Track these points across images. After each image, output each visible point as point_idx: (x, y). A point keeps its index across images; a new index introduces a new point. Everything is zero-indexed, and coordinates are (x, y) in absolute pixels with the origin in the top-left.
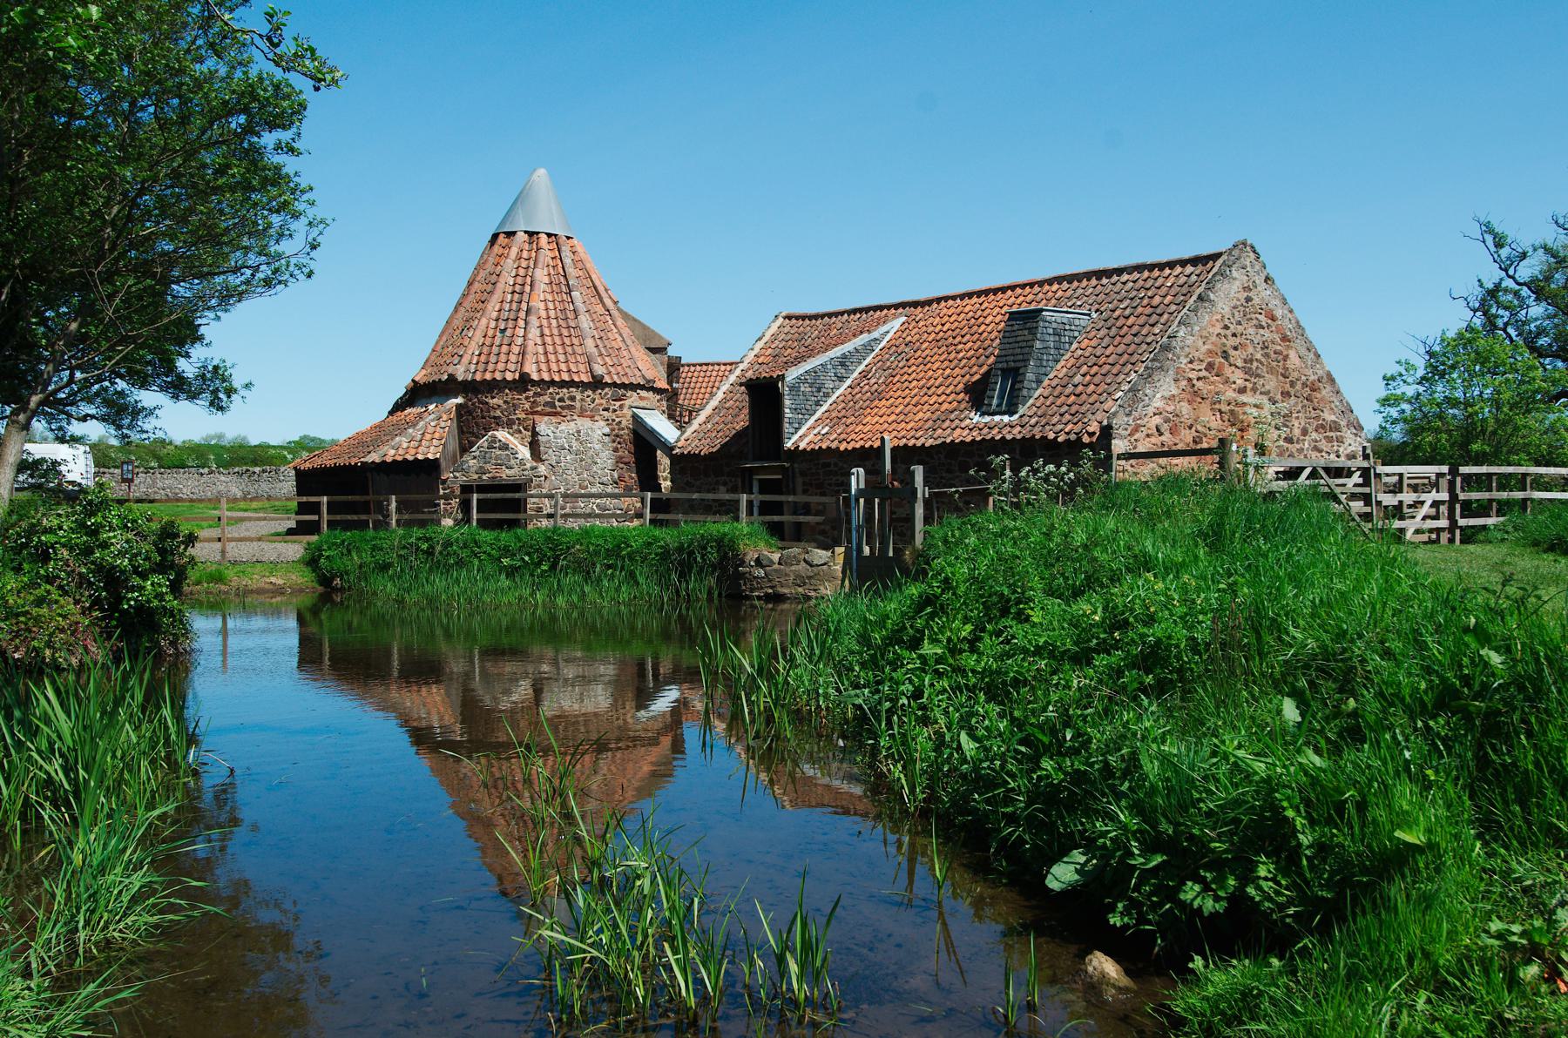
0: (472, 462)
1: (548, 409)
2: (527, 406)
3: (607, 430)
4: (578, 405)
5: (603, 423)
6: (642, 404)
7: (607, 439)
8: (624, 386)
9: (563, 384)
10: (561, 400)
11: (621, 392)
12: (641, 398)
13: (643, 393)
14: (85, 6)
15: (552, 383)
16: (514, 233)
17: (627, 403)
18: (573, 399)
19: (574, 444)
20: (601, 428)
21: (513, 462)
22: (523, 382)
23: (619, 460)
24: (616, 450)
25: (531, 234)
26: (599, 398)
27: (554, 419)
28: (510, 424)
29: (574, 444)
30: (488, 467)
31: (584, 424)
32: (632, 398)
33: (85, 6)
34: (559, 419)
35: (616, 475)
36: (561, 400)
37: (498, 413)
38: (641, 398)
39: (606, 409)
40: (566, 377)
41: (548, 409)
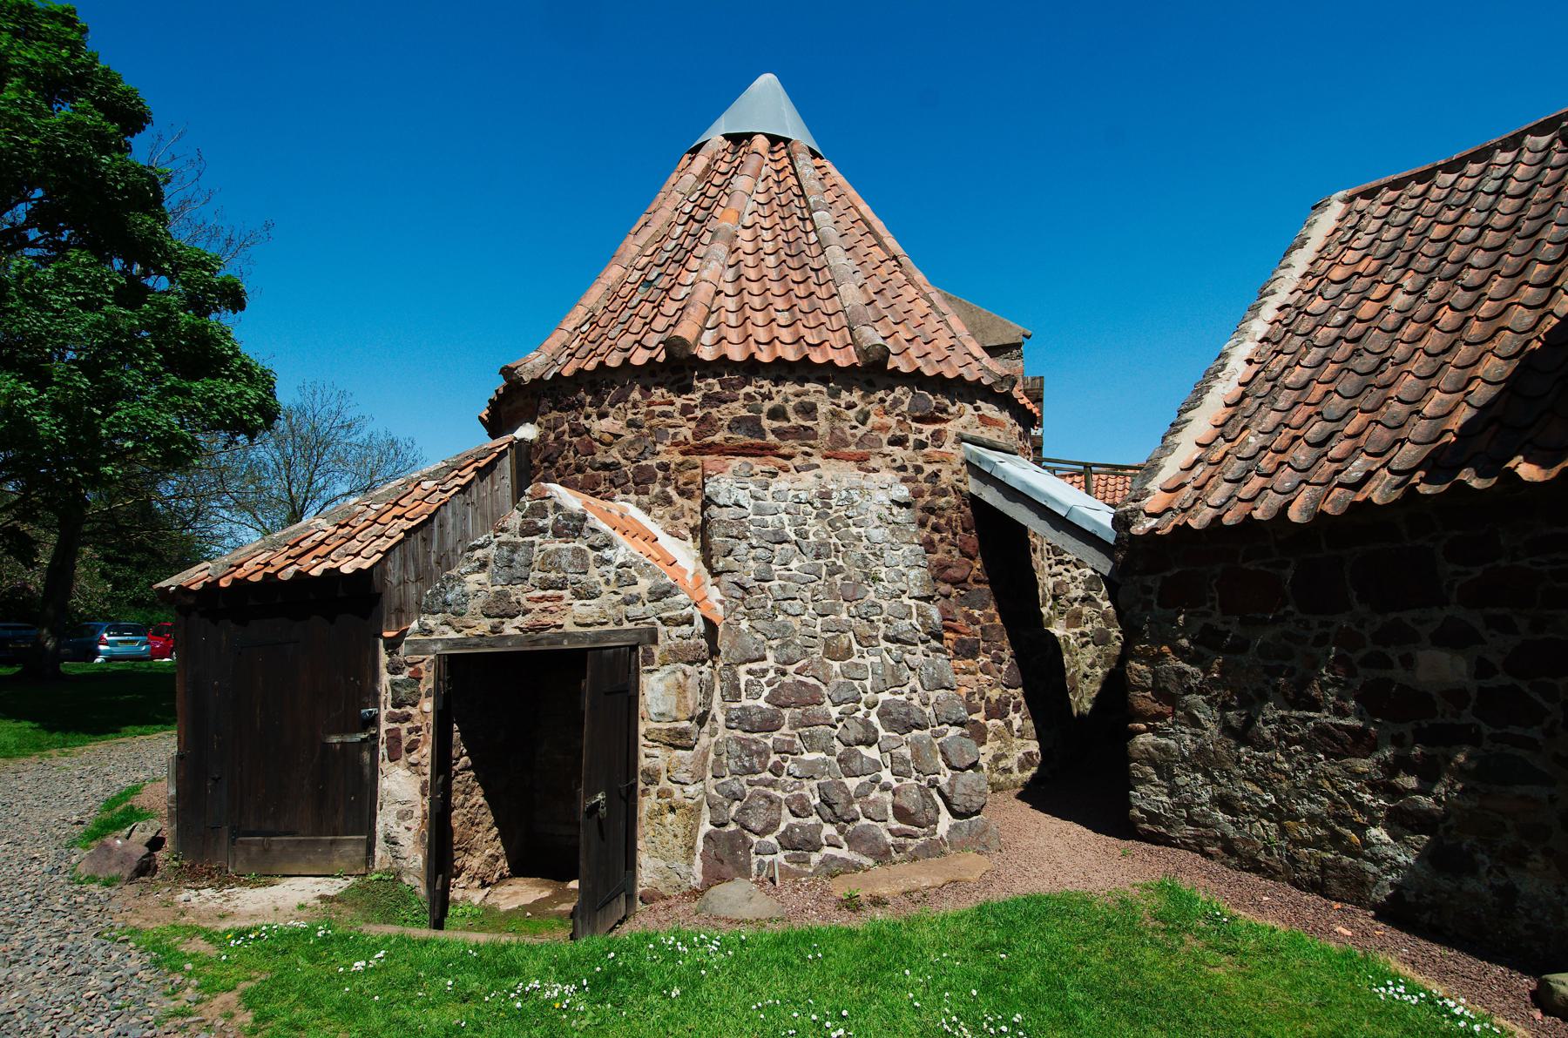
0: (473, 581)
1: (742, 438)
2: (686, 431)
3: (902, 492)
4: (822, 426)
5: (888, 476)
6: (989, 434)
7: (902, 515)
8: (939, 384)
9: (781, 371)
10: (777, 414)
11: (933, 400)
12: (985, 421)
13: (989, 410)
14: (98, 653)
15: (752, 368)
16: (749, 136)
17: (952, 428)
18: (808, 410)
19: (814, 528)
20: (883, 488)
21: (595, 574)
22: (678, 367)
23: (940, 573)
24: (929, 546)
25: (774, 140)
26: (883, 413)
27: (758, 464)
28: (642, 480)
29: (814, 528)
30: (518, 593)
31: (840, 476)
32: (964, 418)
33: (98, 653)
34: (771, 463)
35: (934, 612)
36: (777, 414)
37: (615, 455)
38: (985, 421)
39: (899, 441)
40: (791, 355)
41: (742, 438)
